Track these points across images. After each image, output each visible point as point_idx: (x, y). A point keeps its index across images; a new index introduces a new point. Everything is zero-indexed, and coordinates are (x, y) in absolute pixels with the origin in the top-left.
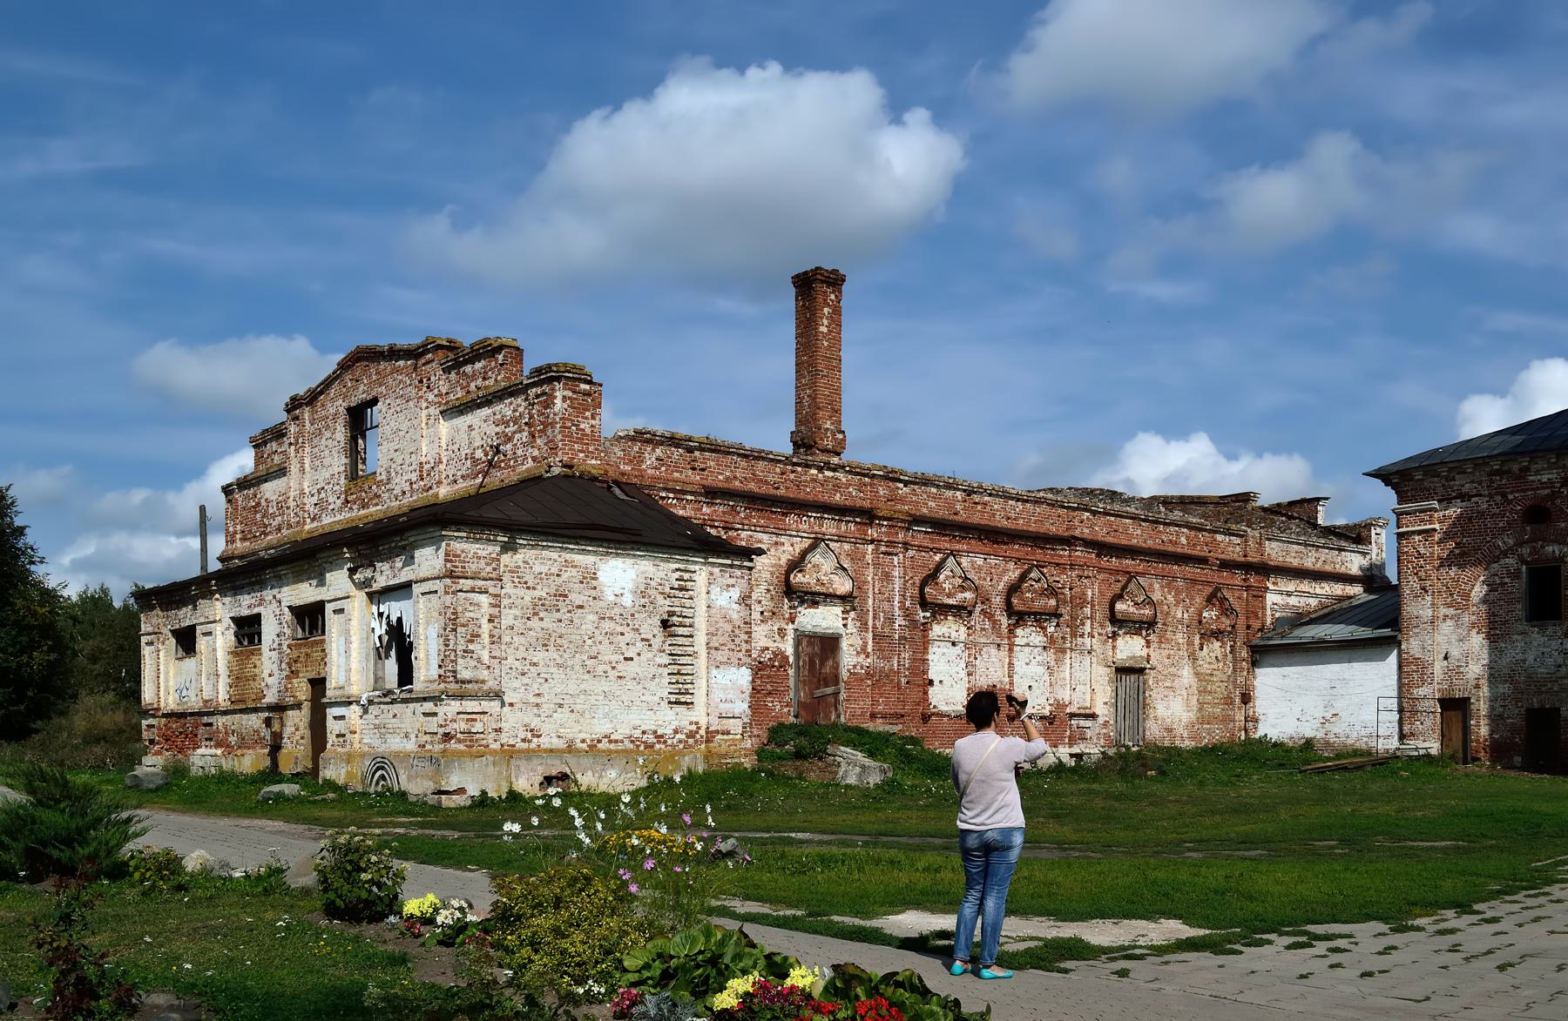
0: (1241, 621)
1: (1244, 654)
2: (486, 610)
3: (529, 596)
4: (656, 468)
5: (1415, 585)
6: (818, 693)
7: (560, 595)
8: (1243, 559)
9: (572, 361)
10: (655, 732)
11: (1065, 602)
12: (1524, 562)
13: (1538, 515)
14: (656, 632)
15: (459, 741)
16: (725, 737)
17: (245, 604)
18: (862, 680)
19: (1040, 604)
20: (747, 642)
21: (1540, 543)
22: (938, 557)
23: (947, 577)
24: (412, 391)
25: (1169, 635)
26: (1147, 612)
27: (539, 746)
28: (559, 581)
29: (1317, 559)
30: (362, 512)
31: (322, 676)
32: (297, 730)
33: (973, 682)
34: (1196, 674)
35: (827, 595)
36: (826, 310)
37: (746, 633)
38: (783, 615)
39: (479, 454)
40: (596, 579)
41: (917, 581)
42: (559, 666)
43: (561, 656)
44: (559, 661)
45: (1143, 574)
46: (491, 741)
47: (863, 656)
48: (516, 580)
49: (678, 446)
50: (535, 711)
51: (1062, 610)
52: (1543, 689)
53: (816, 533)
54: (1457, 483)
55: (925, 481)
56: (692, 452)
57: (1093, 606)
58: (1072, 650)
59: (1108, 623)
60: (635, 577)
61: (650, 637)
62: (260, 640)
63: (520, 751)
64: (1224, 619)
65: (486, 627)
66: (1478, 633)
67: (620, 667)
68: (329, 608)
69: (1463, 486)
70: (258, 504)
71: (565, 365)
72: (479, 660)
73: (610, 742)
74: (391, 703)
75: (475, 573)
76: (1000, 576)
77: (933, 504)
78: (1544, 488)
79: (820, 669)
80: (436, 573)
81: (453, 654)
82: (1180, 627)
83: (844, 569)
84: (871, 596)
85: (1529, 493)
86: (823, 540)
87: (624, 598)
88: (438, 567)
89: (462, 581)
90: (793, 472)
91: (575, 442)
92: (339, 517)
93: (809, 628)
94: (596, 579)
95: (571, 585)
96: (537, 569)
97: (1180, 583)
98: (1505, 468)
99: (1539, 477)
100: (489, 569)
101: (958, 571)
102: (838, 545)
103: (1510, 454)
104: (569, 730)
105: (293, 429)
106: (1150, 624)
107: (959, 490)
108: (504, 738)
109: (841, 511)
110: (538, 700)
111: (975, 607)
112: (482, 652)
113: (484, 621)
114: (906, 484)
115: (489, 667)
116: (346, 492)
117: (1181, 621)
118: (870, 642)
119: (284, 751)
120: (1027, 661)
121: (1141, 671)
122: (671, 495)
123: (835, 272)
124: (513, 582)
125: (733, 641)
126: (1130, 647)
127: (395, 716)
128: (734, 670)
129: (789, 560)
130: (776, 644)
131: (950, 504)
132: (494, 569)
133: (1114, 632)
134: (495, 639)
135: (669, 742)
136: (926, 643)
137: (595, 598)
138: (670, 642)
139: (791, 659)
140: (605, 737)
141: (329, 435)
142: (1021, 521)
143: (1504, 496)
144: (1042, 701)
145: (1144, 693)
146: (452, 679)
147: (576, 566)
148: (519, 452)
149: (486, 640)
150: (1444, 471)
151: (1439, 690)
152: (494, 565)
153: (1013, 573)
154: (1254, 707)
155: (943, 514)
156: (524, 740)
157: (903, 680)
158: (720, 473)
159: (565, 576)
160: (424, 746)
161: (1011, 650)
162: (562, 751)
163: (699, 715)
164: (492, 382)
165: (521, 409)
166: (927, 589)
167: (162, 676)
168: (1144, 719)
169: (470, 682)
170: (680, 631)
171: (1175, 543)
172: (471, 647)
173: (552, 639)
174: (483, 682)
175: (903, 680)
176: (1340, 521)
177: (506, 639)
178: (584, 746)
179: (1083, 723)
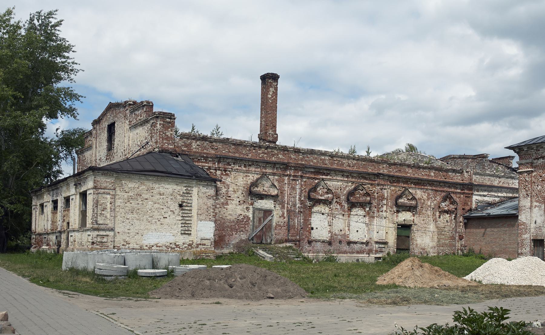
0: (460, 207)
1: (461, 219)
5: (524, 193)
7: (138, 195)
8: (462, 182)
10: (175, 244)
11: (374, 198)
14: (176, 208)
16: (204, 246)
19: (362, 199)
20: (213, 212)
25: (424, 212)
26: (413, 202)
28: (138, 190)
29: (500, 182)
34: (437, 227)
37: (213, 209)
38: (248, 202)
41: (307, 190)
42: (137, 219)
43: (138, 216)
44: (137, 218)
46: (109, 245)
48: (122, 190)
49: (206, 141)
50: (128, 235)
53: (263, 172)
54: (541, 152)
56: (212, 143)
57: (387, 200)
59: (394, 207)
61: (174, 210)
64: (451, 206)
65: (109, 205)
67: (161, 220)
69: (543, 153)
72: (106, 217)
73: (157, 246)
74: (83, 231)
75: (105, 187)
81: (96, 215)
82: (429, 208)
83: (275, 186)
84: (286, 196)
89: (100, 190)
90: (254, 149)
95: (143, 191)
100: (110, 186)
101: (325, 186)
103: (236, 161)
104: (141, 242)
105: (94, 132)
109: (274, 165)
110: (129, 231)
111: (333, 200)
112: (108, 214)
113: (108, 204)
116: (107, 155)
117: (430, 206)
118: (286, 213)
119: (61, 247)
122: (202, 159)
124: (120, 190)
126: (405, 217)
129: (251, 182)
130: (245, 213)
134: (112, 210)
135: (181, 247)
136: (311, 213)
138: (182, 212)
139: (251, 219)
141: (103, 135)
146: (95, 223)
149: (109, 210)
150: (534, 147)
151: (532, 236)
156: (123, 245)
163: (195, 238)
164: (142, 117)
167: (37, 221)
169: (102, 224)
170: (186, 208)
171: (429, 176)
172: (103, 212)
173: (135, 210)
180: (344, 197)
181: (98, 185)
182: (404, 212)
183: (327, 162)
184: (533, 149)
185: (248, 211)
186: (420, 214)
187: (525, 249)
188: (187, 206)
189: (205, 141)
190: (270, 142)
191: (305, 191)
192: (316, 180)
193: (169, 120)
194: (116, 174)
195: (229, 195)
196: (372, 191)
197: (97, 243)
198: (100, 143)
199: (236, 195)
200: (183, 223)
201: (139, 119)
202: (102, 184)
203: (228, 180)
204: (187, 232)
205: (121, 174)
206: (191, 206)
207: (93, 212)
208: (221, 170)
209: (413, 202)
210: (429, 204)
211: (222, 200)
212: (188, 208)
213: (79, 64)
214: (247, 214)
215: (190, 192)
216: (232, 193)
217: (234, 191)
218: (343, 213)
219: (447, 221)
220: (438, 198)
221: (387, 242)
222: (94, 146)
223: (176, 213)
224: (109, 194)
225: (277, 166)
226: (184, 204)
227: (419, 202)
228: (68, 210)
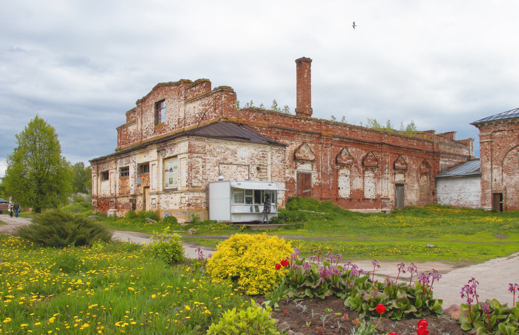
0: (432, 169)
1: (433, 179)
2: (201, 164)
4: (254, 119)
6: (304, 191)
7: (225, 159)
15: (193, 206)
17: (122, 163)
20: (284, 174)
22: (341, 149)
23: (344, 155)
24: (176, 97)
25: (411, 174)
26: (404, 166)
28: (225, 154)
29: (454, 150)
30: (160, 135)
31: (148, 185)
32: (140, 203)
33: (352, 188)
34: (419, 186)
35: (307, 160)
37: (284, 171)
39: (197, 115)
41: (335, 156)
45: (403, 155)
47: (318, 180)
49: (260, 113)
51: (379, 166)
57: (388, 165)
58: (382, 178)
61: (253, 173)
62: (129, 175)
64: (427, 169)
68: (150, 164)
70: (127, 133)
76: (360, 155)
80: (185, 151)
83: (313, 152)
88: (186, 150)
89: (194, 154)
90: (296, 121)
92: (152, 137)
96: (218, 150)
97: (414, 157)
98: (513, 122)
100: (202, 150)
113: (201, 167)
115: (202, 182)
117: (414, 169)
123: (309, 59)
126: (399, 178)
127: (172, 198)
132: (204, 150)
133: (395, 173)
136: (337, 176)
139: (296, 181)
144: (373, 194)
147: (230, 150)
148: (210, 115)
153: (364, 154)
157: (331, 188)
159: (226, 153)
160: (181, 208)
161: (363, 178)
165: (211, 101)
166: (338, 159)
170: (263, 171)
174: (200, 187)
177: (208, 173)
180: (360, 162)
182: (399, 174)
183: (347, 133)
188: (263, 169)
190: (307, 115)
191: (334, 157)
193: (232, 94)
194: (207, 139)
201: (197, 95)
206: (266, 169)
207: (189, 175)
209: (404, 166)
215: (266, 155)
223: (255, 176)
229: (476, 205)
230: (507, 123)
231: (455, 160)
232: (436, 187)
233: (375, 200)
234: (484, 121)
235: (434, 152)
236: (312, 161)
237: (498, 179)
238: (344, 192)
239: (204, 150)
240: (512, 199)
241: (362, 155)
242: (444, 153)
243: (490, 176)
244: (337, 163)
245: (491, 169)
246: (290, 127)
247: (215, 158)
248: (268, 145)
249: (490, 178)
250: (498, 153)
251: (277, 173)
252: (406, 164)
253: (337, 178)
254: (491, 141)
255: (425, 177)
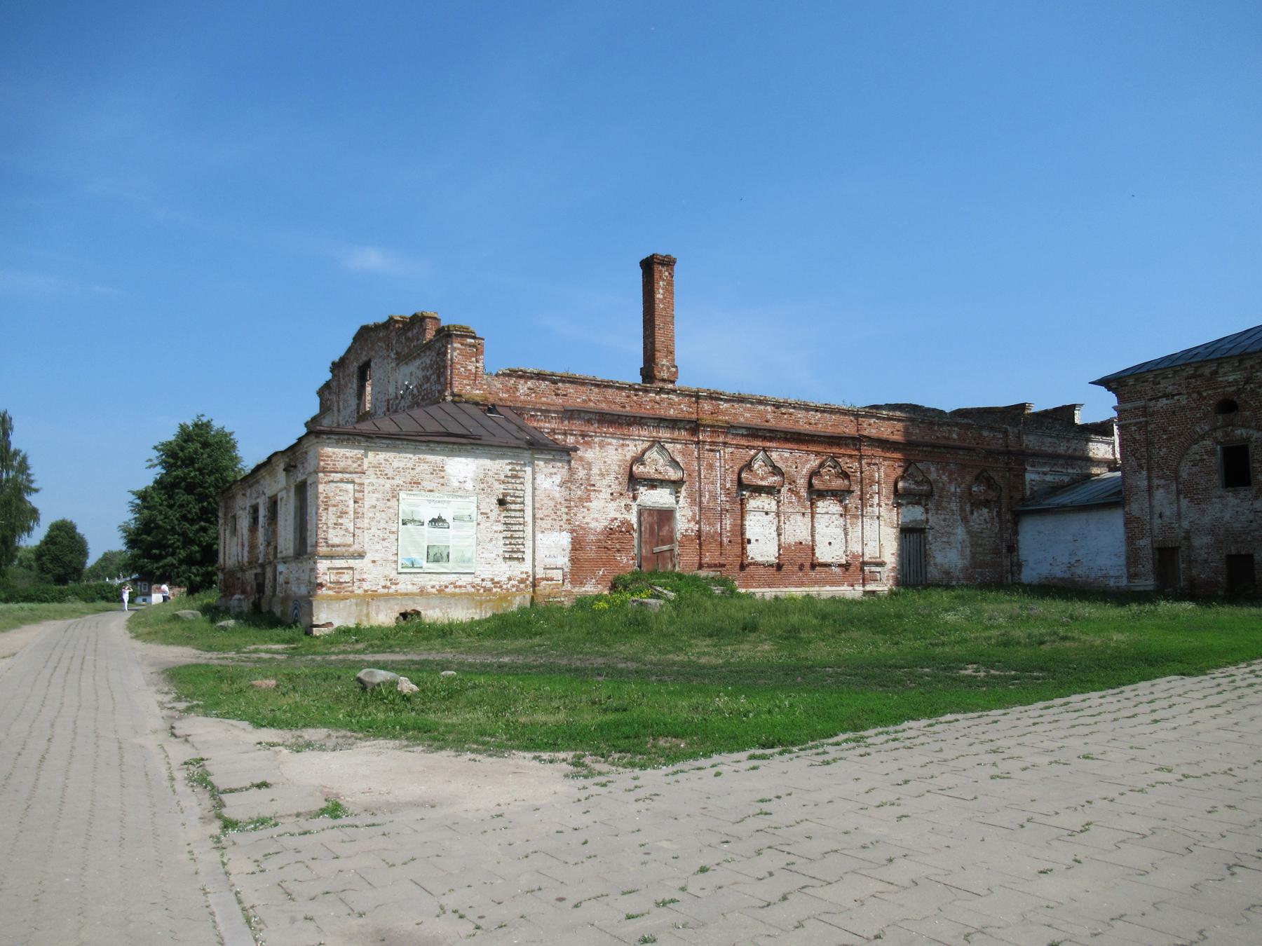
1: (1009, 517)
3: (388, 484)
4: (528, 395)
6: (656, 550)
7: (414, 483)
8: (1005, 449)
9: (464, 324)
12: (1218, 443)
13: (1228, 407)
14: (493, 508)
15: (330, 589)
16: (550, 582)
18: (692, 540)
20: (567, 514)
21: (1230, 428)
23: (760, 466)
25: (944, 504)
27: (396, 591)
29: (1068, 448)
34: (969, 532)
36: (661, 283)
37: (567, 507)
40: (443, 471)
41: (736, 469)
45: (921, 461)
49: (544, 380)
52: (1239, 539)
53: (654, 437)
55: (741, 400)
60: (475, 469)
61: (488, 511)
63: (380, 595)
64: (990, 492)
66: (1185, 498)
71: (454, 326)
72: (347, 530)
73: (455, 587)
77: (748, 415)
78: (1230, 386)
79: (658, 533)
81: (325, 526)
82: (954, 498)
85: (1219, 390)
86: (659, 442)
87: (467, 484)
89: (333, 474)
90: (636, 395)
91: (464, 379)
93: (649, 503)
94: (443, 471)
97: (952, 466)
98: (1199, 372)
99: (1226, 378)
100: (355, 465)
102: (672, 445)
105: (335, 384)
106: (929, 495)
107: (769, 405)
108: (366, 586)
109: (673, 423)
113: (351, 502)
114: (726, 401)
117: (954, 494)
120: (827, 524)
121: (922, 531)
122: (539, 414)
125: (556, 513)
128: (556, 534)
129: (633, 457)
131: (762, 415)
134: (360, 515)
135: (504, 586)
137: (443, 485)
139: (635, 526)
140: (451, 584)
142: (820, 425)
143: (1199, 393)
144: (841, 552)
145: (925, 546)
146: (323, 544)
150: (1150, 376)
152: (359, 463)
153: (813, 462)
154: (1018, 555)
155: (757, 422)
156: (384, 587)
158: (577, 397)
159: (418, 469)
161: (813, 517)
162: (416, 595)
166: (743, 475)
168: (926, 566)
170: (513, 506)
171: (948, 439)
172: (340, 521)
175: (725, 539)
176: (1090, 421)
178: (434, 590)
179: (873, 569)
180: (802, 481)
181: (329, 465)
182: (910, 507)
183: (769, 416)
184: (1147, 381)
185: (628, 511)
186: (938, 510)
187: (1143, 567)
189: (542, 380)
190: (664, 380)
192: (750, 450)
193: (473, 341)
194: (367, 441)
195: (592, 483)
196: (851, 468)
197: (329, 585)
198: (346, 401)
199: (605, 482)
200: (506, 538)
202: (337, 463)
203: (589, 454)
204: (515, 555)
205: (377, 440)
206: (523, 503)
208: (575, 435)
210: (953, 489)
211: (579, 493)
212: (518, 507)
213: (595, 856)
214: (628, 517)
215: (520, 474)
216: (598, 478)
217: (602, 475)
218: (803, 510)
219: (985, 520)
220: (968, 478)
221: (883, 562)
222: (335, 409)
224: (353, 482)
225: (681, 425)
226: (509, 499)
227: (934, 487)
228: (276, 524)
229: (1116, 577)
230: (1185, 374)
231: (1070, 471)
232: (1016, 533)
233: (846, 567)
234: (1126, 374)
235: (1009, 453)
236: (674, 482)
237: (1167, 513)
238: (763, 548)
239: (359, 465)
240: (1206, 561)
241: (808, 466)
242: (1037, 455)
243: (1147, 505)
244: (741, 485)
245: (1150, 489)
246: (619, 408)
247: (391, 482)
248: (526, 449)
249: (1147, 510)
250: (1164, 450)
251: (550, 511)
252: (929, 482)
253: (742, 518)
254: (1146, 422)
255: (985, 511)
